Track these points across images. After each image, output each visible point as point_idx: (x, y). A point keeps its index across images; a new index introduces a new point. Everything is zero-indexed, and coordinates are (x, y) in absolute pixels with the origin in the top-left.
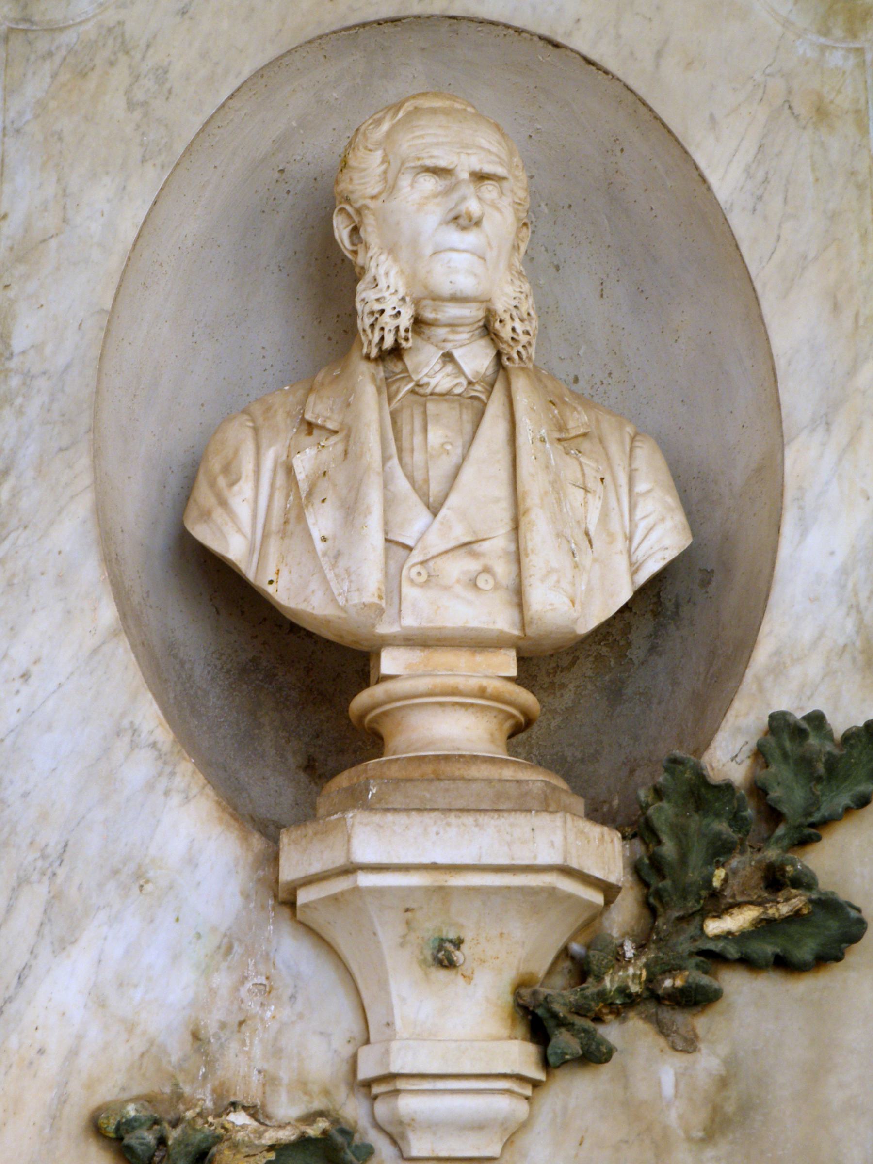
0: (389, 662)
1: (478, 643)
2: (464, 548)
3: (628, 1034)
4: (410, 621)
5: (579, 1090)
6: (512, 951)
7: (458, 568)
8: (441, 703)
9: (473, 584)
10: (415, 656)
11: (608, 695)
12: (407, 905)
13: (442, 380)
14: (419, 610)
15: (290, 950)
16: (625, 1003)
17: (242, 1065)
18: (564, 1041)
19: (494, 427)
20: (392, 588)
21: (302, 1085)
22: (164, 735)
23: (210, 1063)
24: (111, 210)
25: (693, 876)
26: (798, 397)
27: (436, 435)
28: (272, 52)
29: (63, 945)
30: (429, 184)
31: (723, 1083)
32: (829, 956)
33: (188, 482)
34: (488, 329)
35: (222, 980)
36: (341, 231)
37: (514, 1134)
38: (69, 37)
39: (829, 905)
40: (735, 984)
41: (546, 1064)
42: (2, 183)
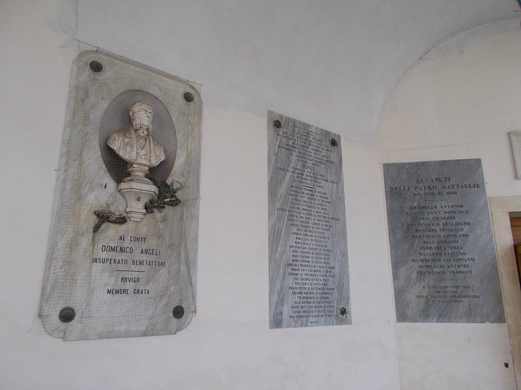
0: (135, 166)
1: (145, 165)
2: (141, 155)
3: (155, 210)
4: (138, 162)
5: (149, 216)
6: (145, 200)
7: (143, 157)
8: (139, 171)
9: (145, 159)
10: (138, 166)
11: (157, 174)
12: (136, 193)
13: (142, 135)
14: (139, 161)
15: (119, 196)
16: (155, 207)
17: (113, 209)
18: (149, 210)
19: (148, 141)
20: (137, 158)
21: (119, 211)
22: (106, 169)
23: (109, 207)
24: (104, 105)
25: (164, 194)
26: (179, 145)
27: (141, 141)
28: (125, 90)
29: (92, 191)
30: (144, 112)
31: (164, 217)
32: (177, 205)
33: (107, 139)
34: (147, 130)
35: (111, 199)
36: (131, 114)
37: (142, 219)
38: (100, 82)
39: (177, 199)
40: (166, 206)
41: (147, 212)
42: (515, 247)
